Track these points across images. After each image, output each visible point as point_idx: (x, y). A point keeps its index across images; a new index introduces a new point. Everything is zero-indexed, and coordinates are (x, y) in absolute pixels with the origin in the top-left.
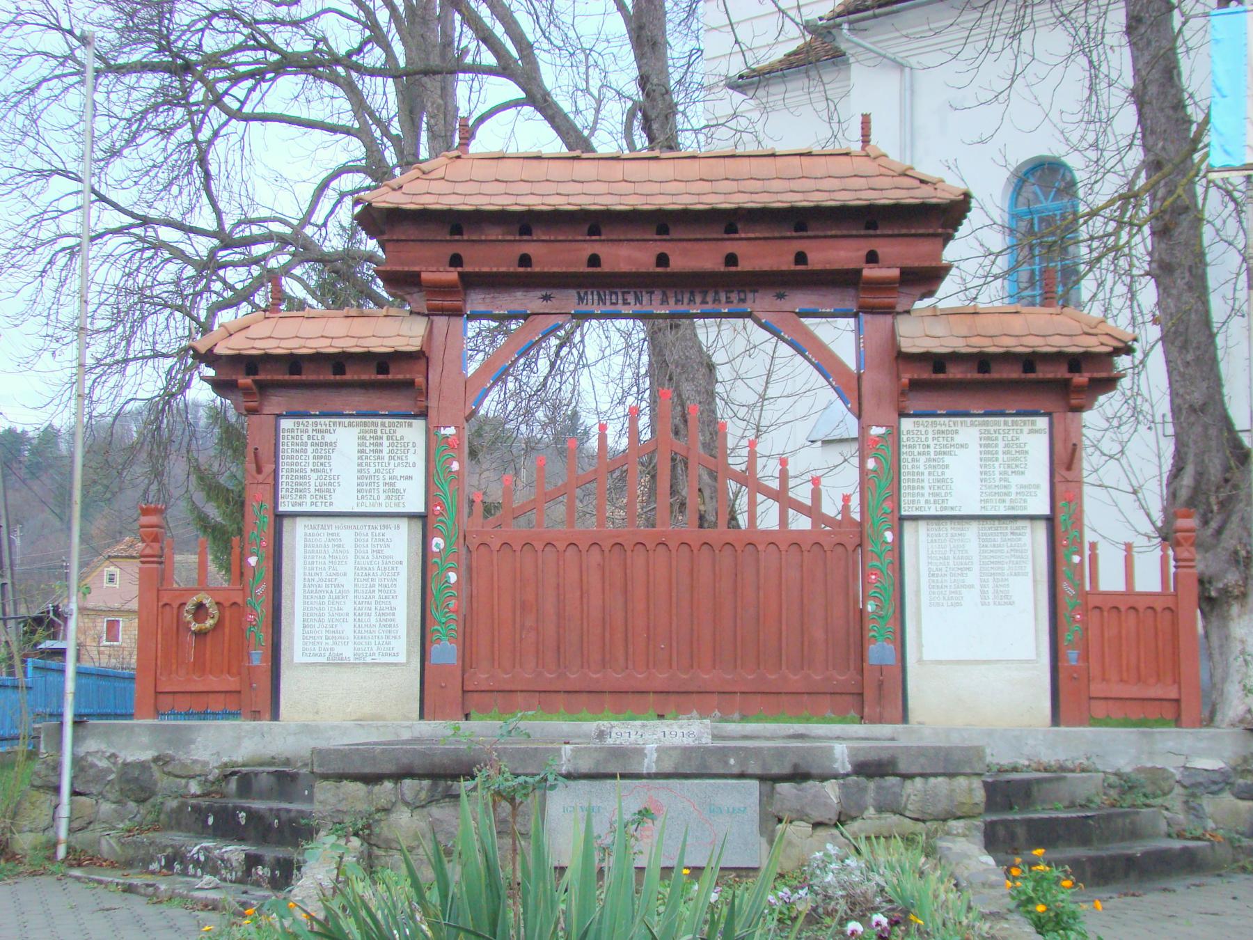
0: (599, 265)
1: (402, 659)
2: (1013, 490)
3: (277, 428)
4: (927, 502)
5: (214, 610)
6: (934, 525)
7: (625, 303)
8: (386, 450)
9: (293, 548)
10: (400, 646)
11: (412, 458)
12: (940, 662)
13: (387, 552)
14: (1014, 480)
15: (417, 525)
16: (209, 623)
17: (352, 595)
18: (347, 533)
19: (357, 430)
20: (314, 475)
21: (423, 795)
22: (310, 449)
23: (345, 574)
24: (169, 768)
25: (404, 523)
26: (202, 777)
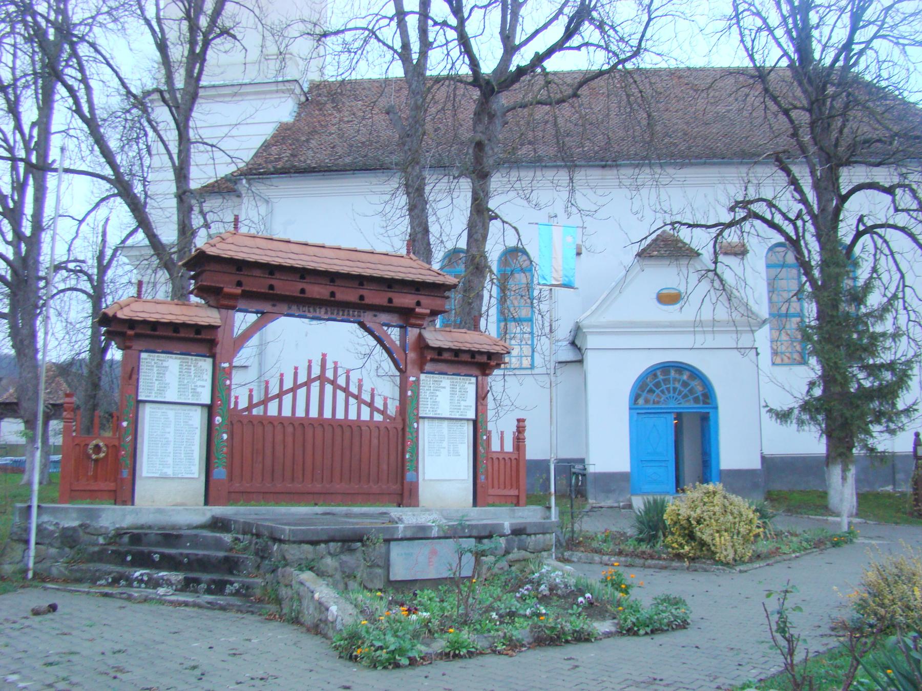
1: (196, 475)
3: (139, 357)
5: (104, 449)
6: (430, 421)
7: (309, 312)
8: (193, 372)
10: (195, 469)
11: (205, 377)
12: (431, 480)
13: (190, 422)
14: (463, 403)
15: (206, 411)
16: (102, 455)
20: (157, 382)
21: (338, 550)
22: (155, 369)
24: (88, 530)
25: (199, 409)
26: (105, 535)
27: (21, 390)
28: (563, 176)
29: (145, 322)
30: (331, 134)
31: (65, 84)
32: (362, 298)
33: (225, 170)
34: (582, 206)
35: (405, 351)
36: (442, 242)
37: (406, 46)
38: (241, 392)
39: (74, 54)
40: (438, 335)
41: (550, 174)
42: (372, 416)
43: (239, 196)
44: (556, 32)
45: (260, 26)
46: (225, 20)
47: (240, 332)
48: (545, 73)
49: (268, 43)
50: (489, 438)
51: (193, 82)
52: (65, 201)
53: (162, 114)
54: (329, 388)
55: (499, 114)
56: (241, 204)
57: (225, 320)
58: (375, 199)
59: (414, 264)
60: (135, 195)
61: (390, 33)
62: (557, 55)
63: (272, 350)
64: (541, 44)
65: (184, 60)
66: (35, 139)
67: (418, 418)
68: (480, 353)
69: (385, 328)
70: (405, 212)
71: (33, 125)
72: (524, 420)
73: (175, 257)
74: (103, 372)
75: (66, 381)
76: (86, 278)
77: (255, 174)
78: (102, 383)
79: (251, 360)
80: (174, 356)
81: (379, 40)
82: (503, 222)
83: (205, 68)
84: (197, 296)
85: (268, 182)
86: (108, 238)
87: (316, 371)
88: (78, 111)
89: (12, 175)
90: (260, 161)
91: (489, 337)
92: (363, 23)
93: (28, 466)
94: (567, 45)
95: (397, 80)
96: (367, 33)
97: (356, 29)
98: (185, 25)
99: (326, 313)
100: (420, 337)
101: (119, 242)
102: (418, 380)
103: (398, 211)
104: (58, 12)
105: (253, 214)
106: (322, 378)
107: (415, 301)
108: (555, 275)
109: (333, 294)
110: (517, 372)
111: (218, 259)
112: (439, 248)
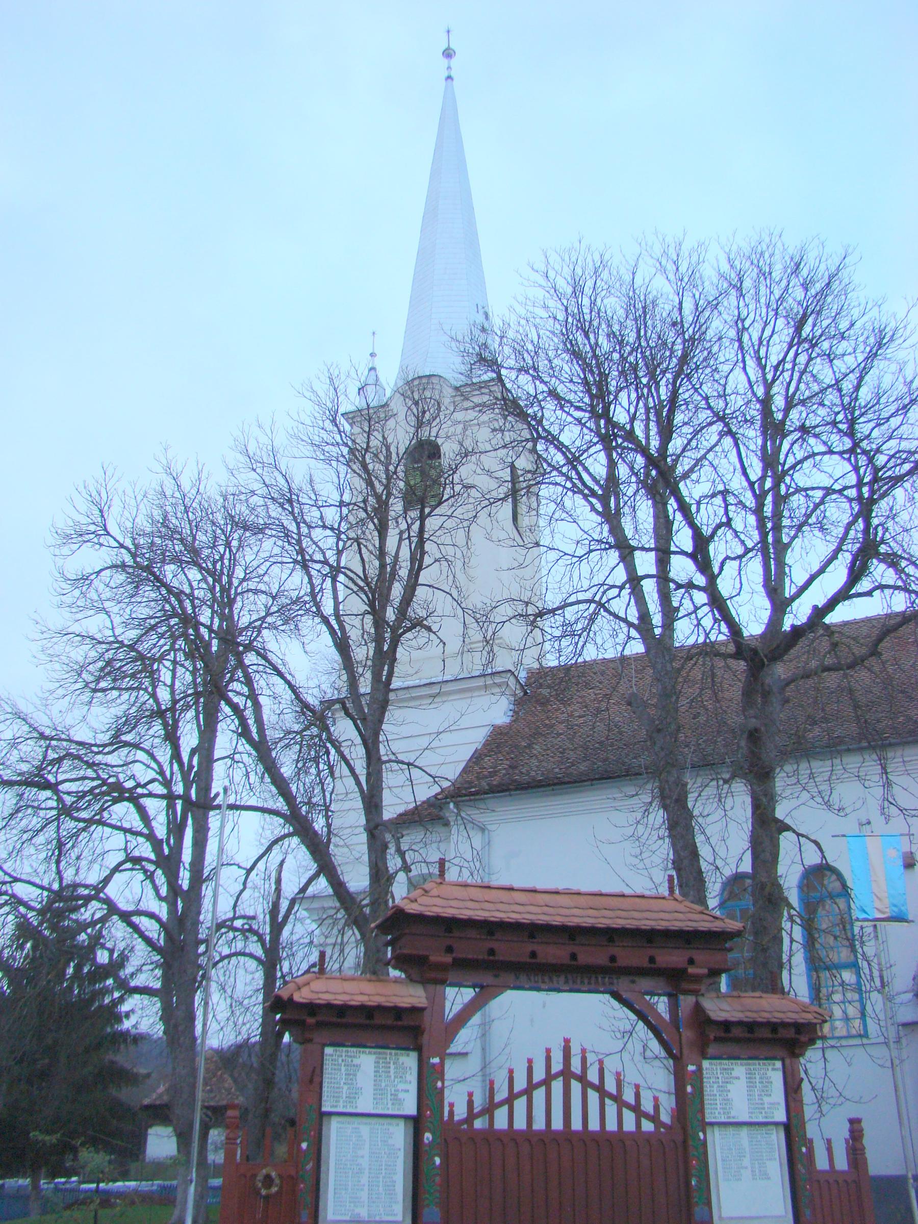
0: (615, 962)
1: (399, 1218)
2: (766, 1106)
3: (323, 1053)
4: (719, 1113)
5: (277, 1181)
6: (756, 1131)
7: (543, 982)
9: (329, 1136)
12: (732, 1218)
13: (390, 1141)
16: (274, 1189)
17: (367, 1171)
18: (365, 1128)
19: (374, 1057)
20: (346, 1087)
22: (343, 1068)
23: (363, 1157)
27: (174, 1090)
28: (870, 765)
29: (329, 1006)
30: (559, 734)
31: (230, 703)
32: (613, 959)
33: (426, 792)
34: (903, 805)
35: (678, 1029)
36: (717, 868)
37: (644, 616)
38: (457, 1098)
39: (241, 664)
40: (723, 1004)
41: (852, 761)
42: (638, 1124)
43: (447, 824)
44: (837, 576)
45: (460, 611)
46: (417, 610)
47: (450, 1017)
48: (827, 627)
49: (471, 632)
50: (811, 1150)
51: (381, 686)
52: (231, 846)
53: (345, 729)
54: (576, 1086)
55: (775, 690)
56: (448, 839)
57: (432, 999)
58: (621, 818)
59: (680, 907)
60: (316, 833)
61: (622, 604)
62: (840, 608)
63: (499, 1030)
64: (817, 595)
65: (369, 663)
66: (195, 769)
67: (705, 1125)
68: (784, 1025)
69: (647, 998)
70: (663, 832)
71: (193, 752)
72: (859, 1121)
73: (367, 910)
74: (279, 1064)
75: (231, 1076)
76: (255, 938)
77: (466, 795)
78: (277, 1079)
79: (472, 1044)
80: (367, 1050)
81: (610, 613)
82: (798, 835)
83: (396, 669)
84: (395, 968)
85: (482, 805)
86: (284, 885)
87: (557, 1066)
88: (244, 733)
89: (168, 815)
90: (470, 777)
91: (795, 1002)
92: (588, 595)
93: (179, 1196)
94: (853, 591)
95: (637, 658)
96: (593, 606)
97: (578, 602)
98: (369, 619)
99: (566, 982)
100: (698, 1009)
101: (297, 890)
102: (700, 1069)
103: (653, 832)
104: (223, 617)
105: (465, 849)
106: (566, 1073)
107: (686, 958)
108: (878, 904)
109: (574, 956)
110: (844, 1042)
111: (420, 918)
112: (713, 879)
